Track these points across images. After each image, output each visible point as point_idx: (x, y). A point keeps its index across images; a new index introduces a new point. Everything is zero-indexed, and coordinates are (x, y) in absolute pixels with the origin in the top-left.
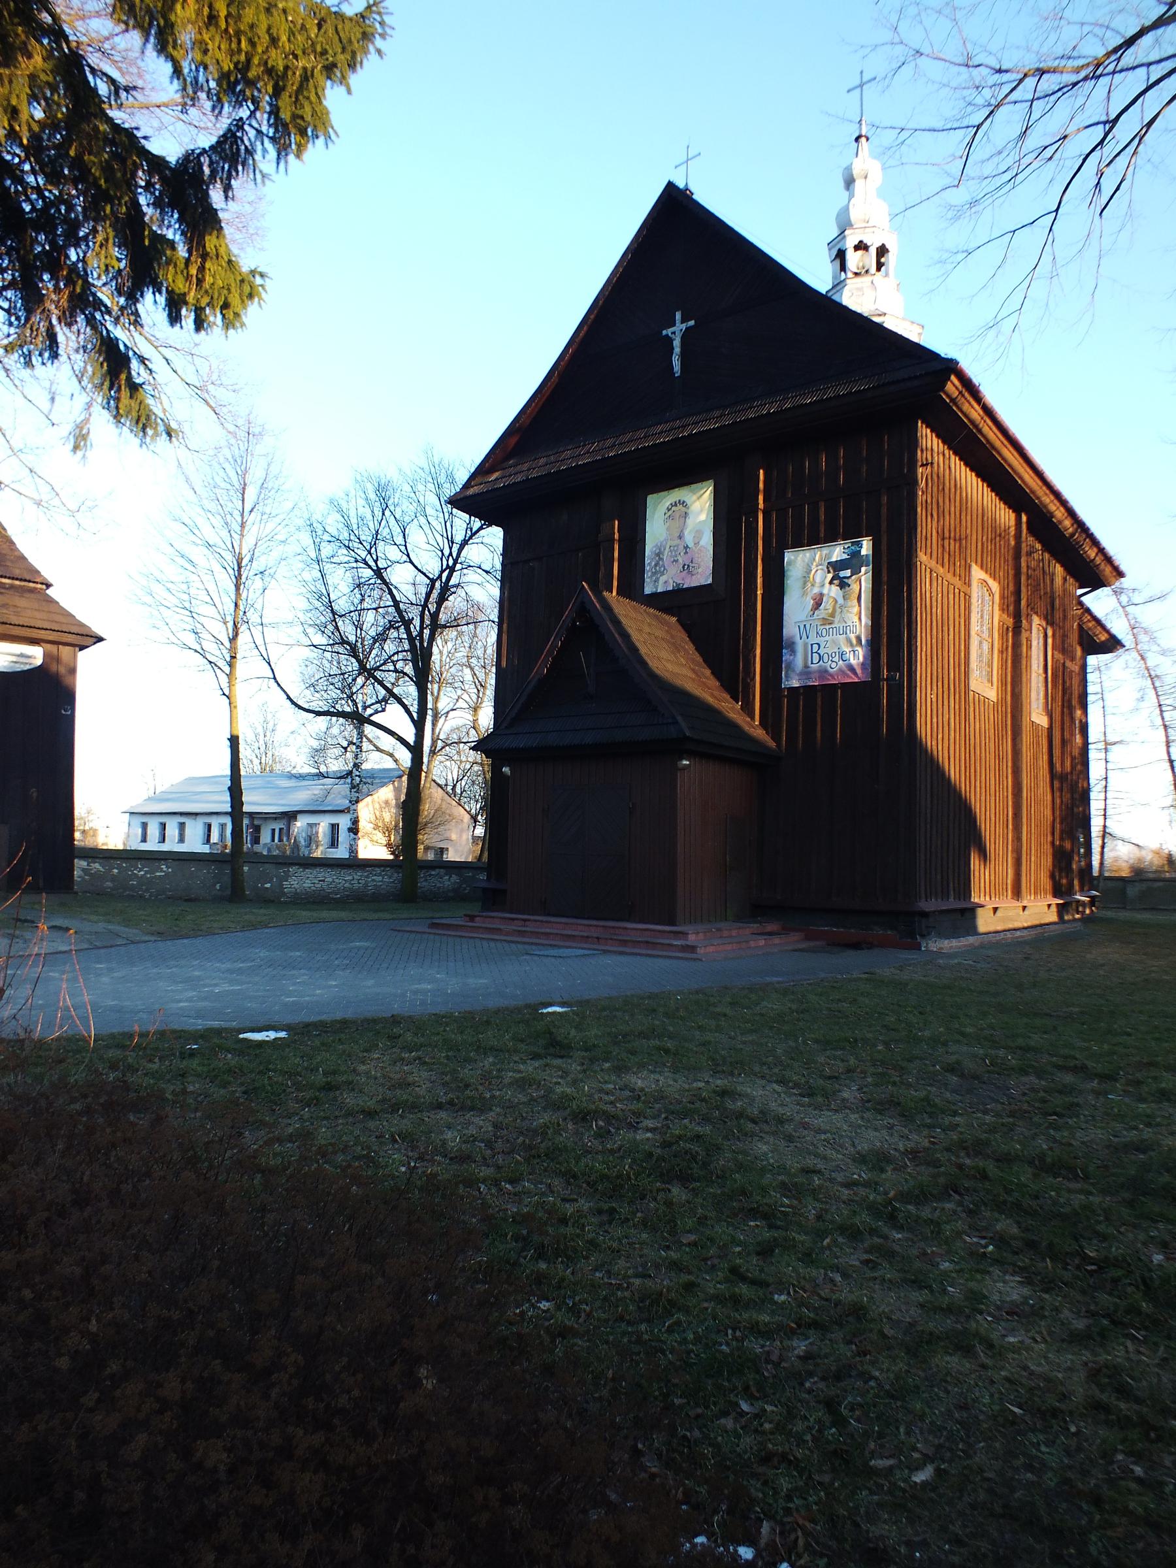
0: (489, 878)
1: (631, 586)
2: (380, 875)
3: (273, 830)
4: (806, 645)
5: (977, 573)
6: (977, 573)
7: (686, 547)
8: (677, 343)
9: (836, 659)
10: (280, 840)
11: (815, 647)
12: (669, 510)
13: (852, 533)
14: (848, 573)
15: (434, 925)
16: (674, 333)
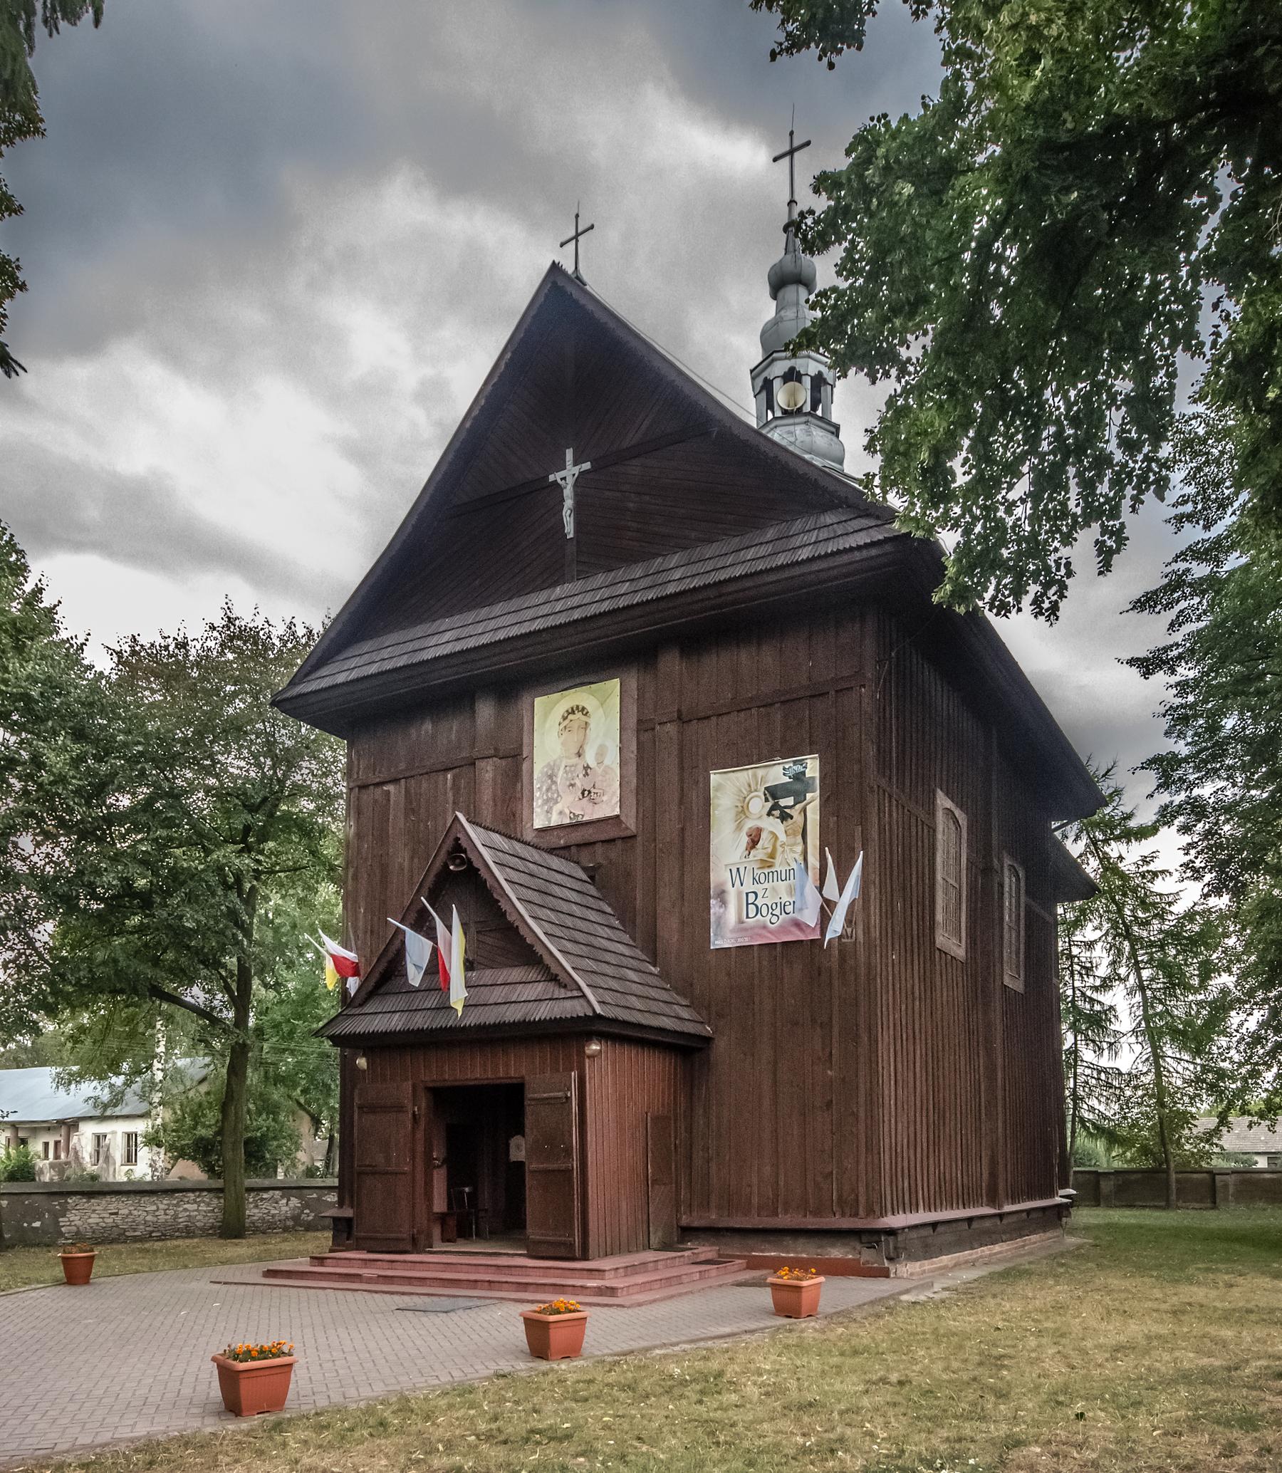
0: (341, 1203)
1: (508, 819)
2: (195, 1202)
3: (46, 1144)
4: (739, 893)
5: (943, 801)
6: (943, 801)
7: (587, 768)
8: (568, 492)
9: (777, 912)
10: (57, 1156)
11: (752, 897)
12: (565, 718)
13: (790, 750)
14: (789, 801)
15: (270, 1273)
16: (564, 479)
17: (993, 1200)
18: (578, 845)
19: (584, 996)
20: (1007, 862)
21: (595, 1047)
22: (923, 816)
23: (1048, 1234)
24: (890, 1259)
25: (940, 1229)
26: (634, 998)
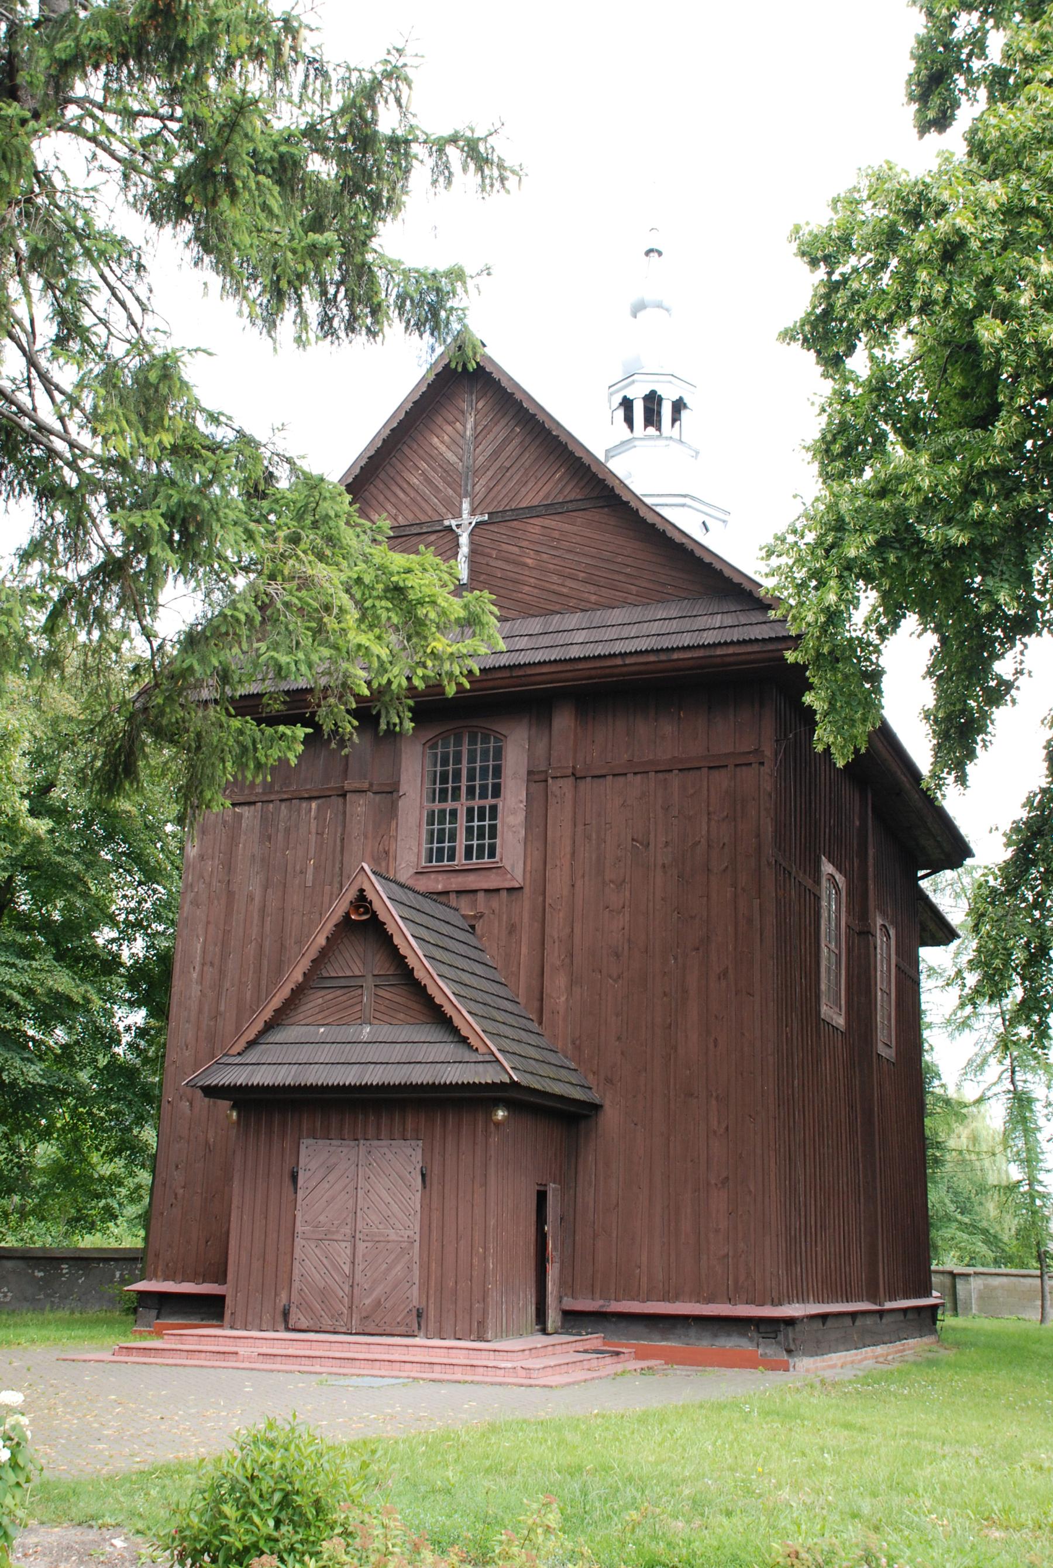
17: (873, 1298)
18: (458, 892)
19: (498, 1061)
20: (879, 921)
21: (501, 1114)
22: (809, 883)
23: (925, 1339)
24: (789, 1351)
25: (830, 1323)
26: (533, 1062)
